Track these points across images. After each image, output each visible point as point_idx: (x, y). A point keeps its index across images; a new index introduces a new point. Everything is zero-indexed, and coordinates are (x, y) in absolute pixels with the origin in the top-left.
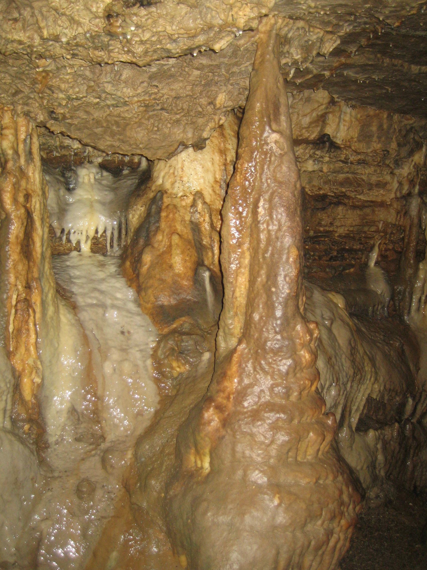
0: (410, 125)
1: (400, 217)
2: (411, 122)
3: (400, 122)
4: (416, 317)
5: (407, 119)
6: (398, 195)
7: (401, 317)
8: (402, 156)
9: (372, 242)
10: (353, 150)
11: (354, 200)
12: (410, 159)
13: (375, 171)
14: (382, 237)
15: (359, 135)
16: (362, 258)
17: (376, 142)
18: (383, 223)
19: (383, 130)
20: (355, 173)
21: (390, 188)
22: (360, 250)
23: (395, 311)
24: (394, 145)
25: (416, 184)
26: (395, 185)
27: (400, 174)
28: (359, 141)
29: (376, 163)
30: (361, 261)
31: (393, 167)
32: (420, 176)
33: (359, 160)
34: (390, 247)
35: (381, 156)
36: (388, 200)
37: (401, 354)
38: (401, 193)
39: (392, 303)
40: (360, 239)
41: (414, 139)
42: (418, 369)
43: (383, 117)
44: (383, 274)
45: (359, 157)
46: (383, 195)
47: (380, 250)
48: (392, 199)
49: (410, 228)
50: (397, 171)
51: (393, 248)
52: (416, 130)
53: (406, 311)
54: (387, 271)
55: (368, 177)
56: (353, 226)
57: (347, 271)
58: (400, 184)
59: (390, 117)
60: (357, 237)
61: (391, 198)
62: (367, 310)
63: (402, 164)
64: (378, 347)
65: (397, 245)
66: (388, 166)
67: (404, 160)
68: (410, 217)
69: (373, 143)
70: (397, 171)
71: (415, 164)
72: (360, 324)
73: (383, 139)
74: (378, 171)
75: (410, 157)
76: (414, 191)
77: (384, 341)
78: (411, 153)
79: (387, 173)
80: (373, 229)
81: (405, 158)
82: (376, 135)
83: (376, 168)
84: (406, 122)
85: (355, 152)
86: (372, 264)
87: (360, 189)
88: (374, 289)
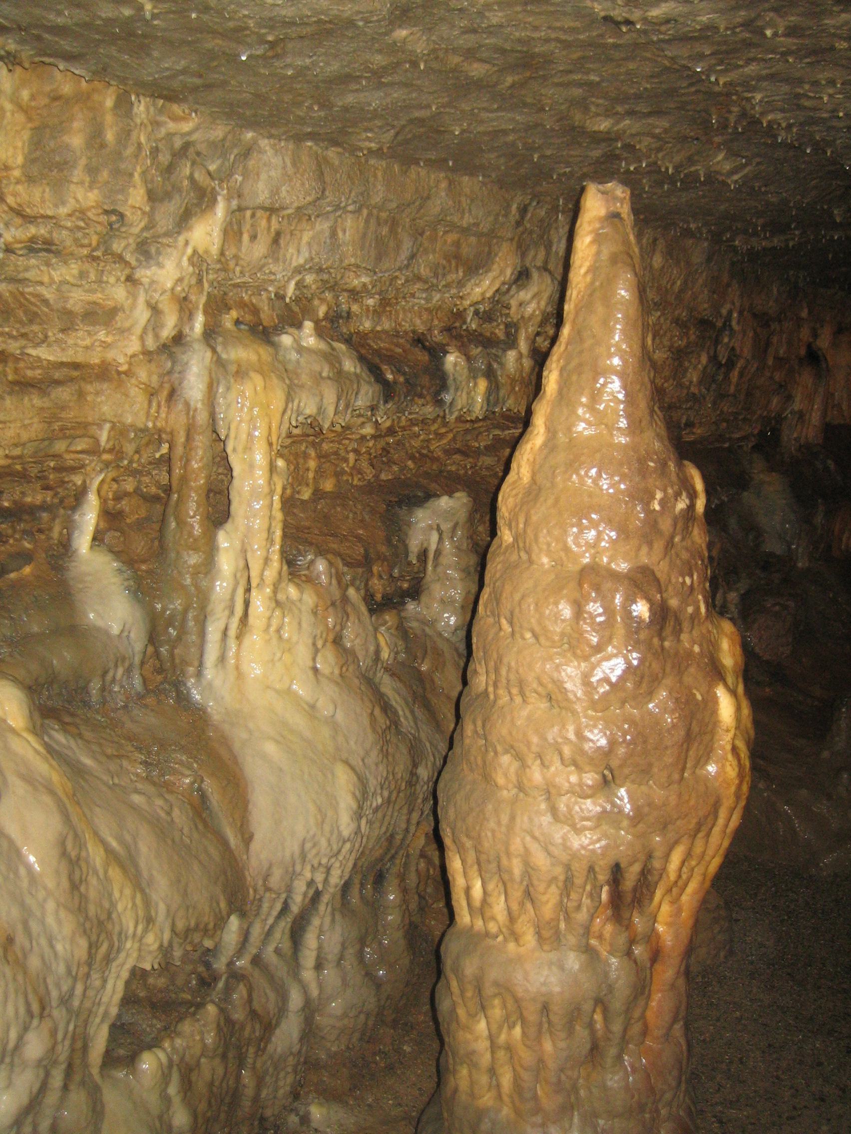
0: (183, 135)
1: (159, 406)
2: (186, 127)
3: (156, 124)
4: (217, 683)
5: (175, 119)
6: (151, 344)
7: (178, 686)
8: (160, 230)
9: (78, 480)
10: (11, 209)
11: (22, 365)
12: (181, 239)
13: (83, 275)
14: (107, 464)
15: (30, 161)
16: (50, 529)
17: (82, 183)
18: (113, 428)
19: (103, 146)
20: (19, 281)
21: (127, 324)
22: (44, 507)
23: (160, 670)
24: (137, 196)
25: (197, 308)
26: (142, 315)
27: (153, 282)
28: (30, 179)
29: (85, 251)
30: (49, 538)
31: (134, 263)
32: (206, 285)
33: (33, 240)
34: (129, 485)
35: (99, 228)
36: (121, 360)
37: (200, 808)
38: (157, 336)
39: (150, 649)
40: (41, 477)
41: (191, 178)
42: (247, 839)
43: (101, 104)
44: (119, 571)
45: (33, 230)
46: (106, 346)
47: (103, 501)
48: (134, 356)
49: (189, 438)
50: (145, 274)
51: (137, 491)
52: (198, 154)
53: (191, 670)
54: (127, 559)
55: (58, 290)
56: (24, 445)
57: (13, 575)
58: (155, 309)
59: (123, 105)
60: (33, 471)
61: (130, 351)
62: (85, 689)
63: (159, 253)
64: (134, 808)
65: (146, 479)
66: (120, 259)
67: (164, 241)
68: (187, 404)
69: (73, 187)
70: (145, 274)
71: (195, 252)
72: (72, 743)
73: (105, 175)
74: (92, 277)
75: (179, 233)
76: (192, 329)
77: (148, 779)
78: (184, 220)
79: (118, 280)
80: (81, 445)
81: (167, 234)
82: (83, 161)
83: (87, 266)
84: (172, 126)
85: (18, 212)
86: (83, 543)
87: (35, 328)
88: (100, 623)
